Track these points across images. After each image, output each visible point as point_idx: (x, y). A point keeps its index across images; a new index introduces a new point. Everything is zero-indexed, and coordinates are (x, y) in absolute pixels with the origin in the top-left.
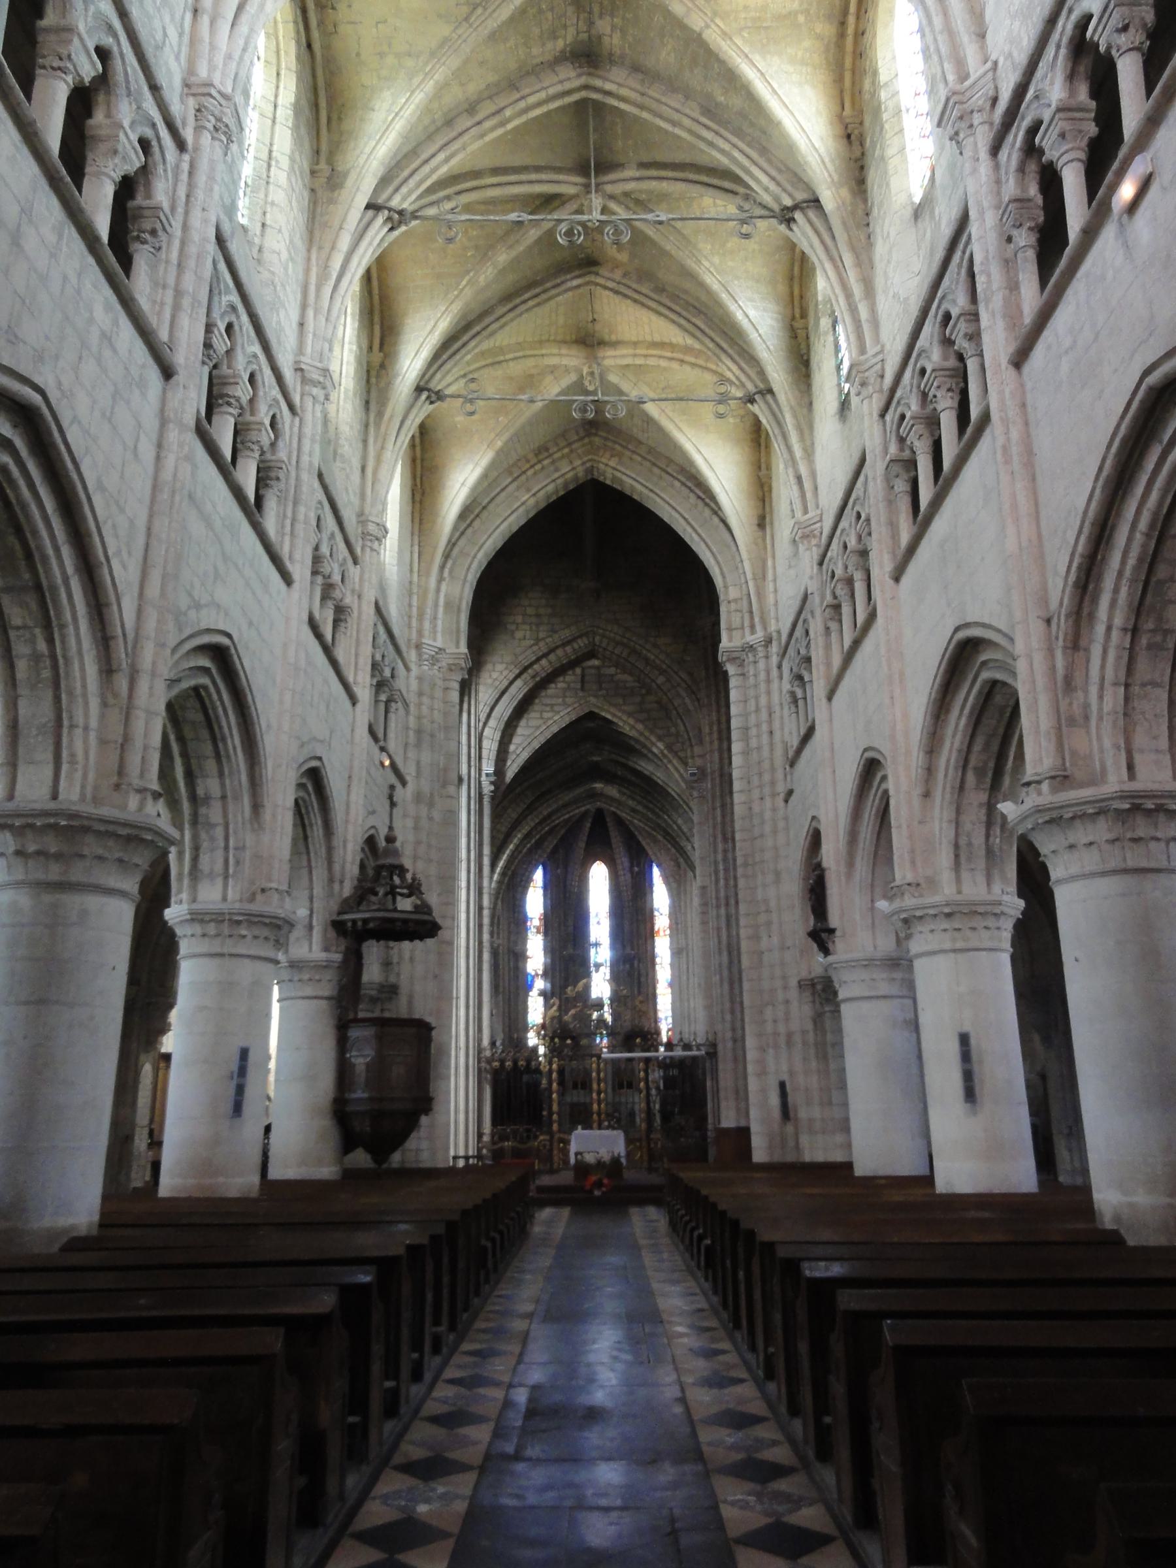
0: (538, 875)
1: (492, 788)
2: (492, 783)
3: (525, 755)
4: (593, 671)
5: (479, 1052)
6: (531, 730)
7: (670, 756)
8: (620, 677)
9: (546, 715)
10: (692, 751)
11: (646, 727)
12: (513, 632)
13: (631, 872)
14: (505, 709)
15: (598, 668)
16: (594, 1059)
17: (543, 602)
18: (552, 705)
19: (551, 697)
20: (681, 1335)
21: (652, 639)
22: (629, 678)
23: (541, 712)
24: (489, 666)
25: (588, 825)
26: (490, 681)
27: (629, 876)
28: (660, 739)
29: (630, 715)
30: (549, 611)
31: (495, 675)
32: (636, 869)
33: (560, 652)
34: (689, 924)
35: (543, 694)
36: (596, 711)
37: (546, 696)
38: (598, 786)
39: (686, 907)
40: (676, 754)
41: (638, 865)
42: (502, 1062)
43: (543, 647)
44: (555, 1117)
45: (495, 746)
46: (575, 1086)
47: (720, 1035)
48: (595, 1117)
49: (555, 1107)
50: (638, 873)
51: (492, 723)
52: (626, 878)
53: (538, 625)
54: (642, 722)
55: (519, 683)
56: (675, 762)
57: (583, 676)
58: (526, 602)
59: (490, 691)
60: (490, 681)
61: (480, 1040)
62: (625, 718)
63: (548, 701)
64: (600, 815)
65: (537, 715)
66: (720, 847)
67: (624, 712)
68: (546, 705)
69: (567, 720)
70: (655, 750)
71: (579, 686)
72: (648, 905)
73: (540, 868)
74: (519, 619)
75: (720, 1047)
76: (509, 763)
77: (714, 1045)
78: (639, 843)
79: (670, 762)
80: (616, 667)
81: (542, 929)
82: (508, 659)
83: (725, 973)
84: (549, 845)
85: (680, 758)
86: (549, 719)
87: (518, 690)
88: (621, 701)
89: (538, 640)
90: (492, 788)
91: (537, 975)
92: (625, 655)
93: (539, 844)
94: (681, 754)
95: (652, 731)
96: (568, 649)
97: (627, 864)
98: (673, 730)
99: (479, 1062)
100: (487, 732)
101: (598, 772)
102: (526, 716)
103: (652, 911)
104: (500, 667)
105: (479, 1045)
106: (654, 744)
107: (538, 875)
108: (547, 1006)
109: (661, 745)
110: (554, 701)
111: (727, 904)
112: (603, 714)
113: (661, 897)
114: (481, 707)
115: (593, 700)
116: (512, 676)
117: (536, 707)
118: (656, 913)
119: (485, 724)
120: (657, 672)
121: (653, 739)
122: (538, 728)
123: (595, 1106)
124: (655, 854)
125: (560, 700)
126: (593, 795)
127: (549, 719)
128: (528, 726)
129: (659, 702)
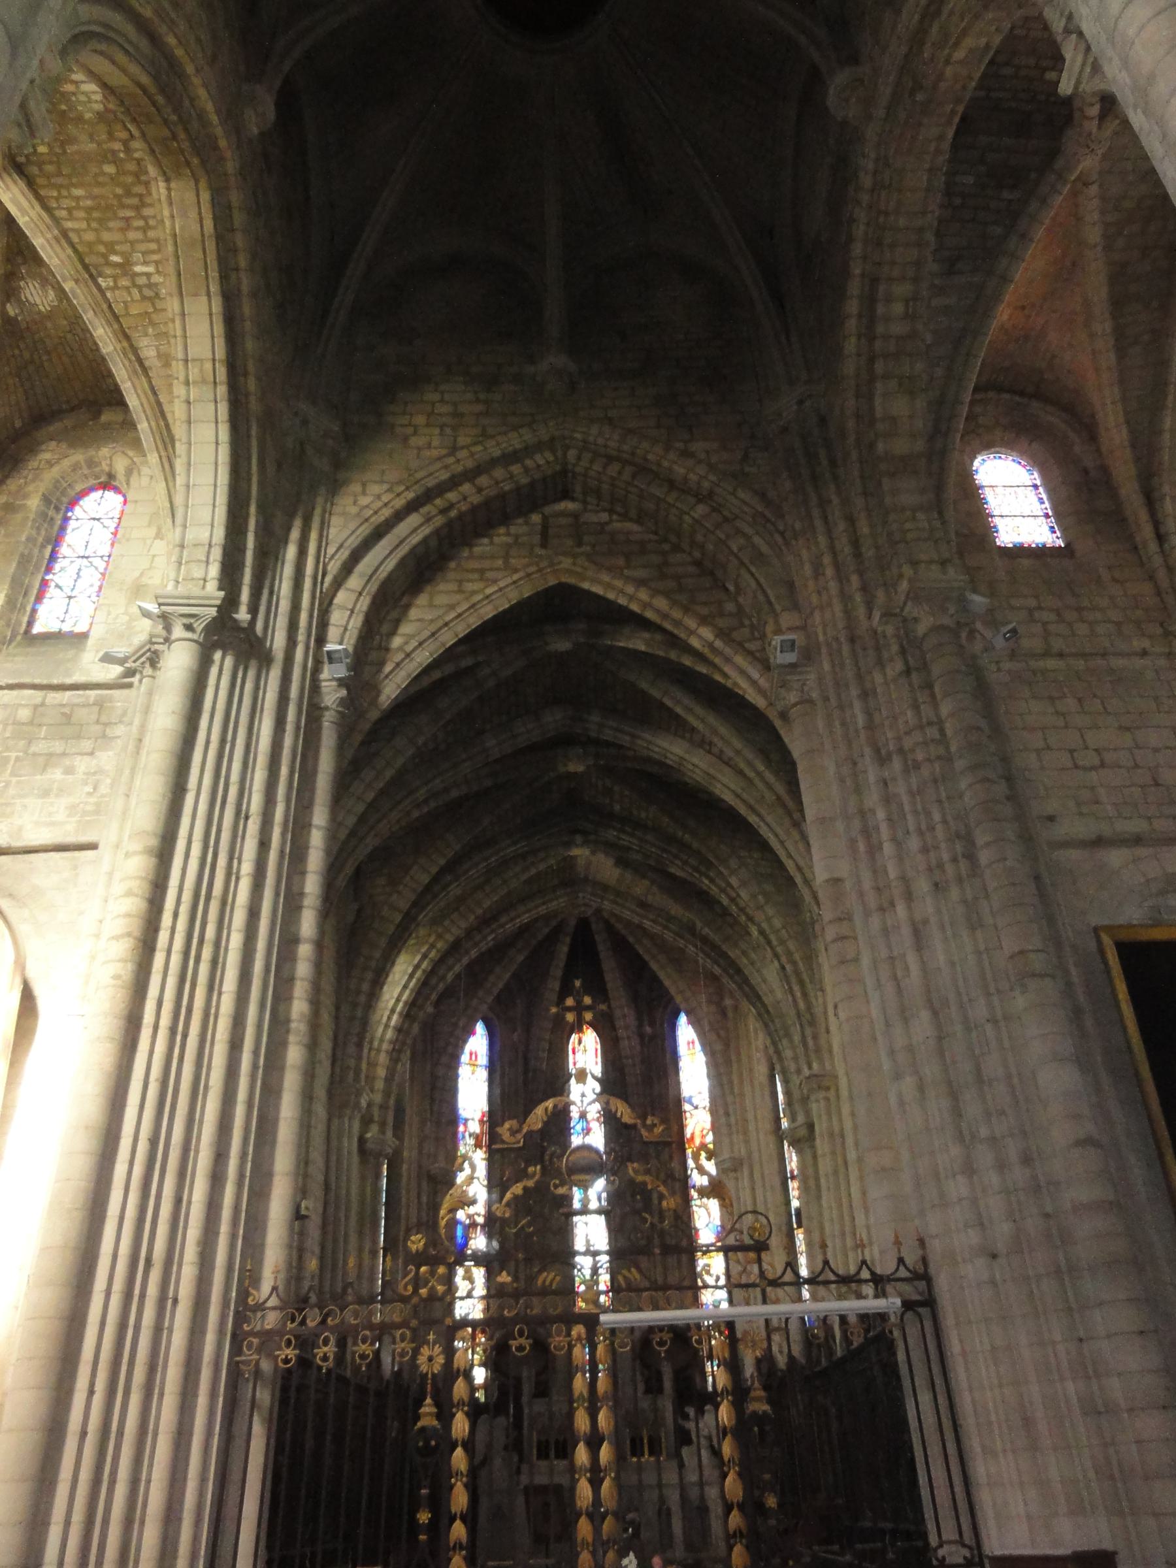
0: (478, 1043)
1: (344, 692)
2: (342, 682)
3: (423, 657)
4: (563, 521)
5: (241, 1318)
6: (440, 612)
7: (728, 651)
8: (617, 525)
9: (469, 586)
10: (777, 622)
11: (674, 603)
12: (406, 439)
13: (641, 1036)
14: (382, 559)
15: (575, 516)
16: (578, 1330)
17: (469, 396)
18: (482, 572)
19: (482, 557)
20: (137, 150)
21: (680, 445)
22: (635, 527)
23: (460, 582)
24: (356, 488)
25: (565, 949)
26: (354, 510)
27: (635, 1042)
28: (704, 620)
29: (641, 583)
30: (479, 408)
31: (364, 501)
32: (648, 1030)
33: (499, 473)
34: (750, 1116)
35: (466, 553)
36: (572, 580)
37: (471, 557)
38: (580, 852)
39: (741, 1082)
40: (740, 646)
41: (652, 1024)
42: (305, 1343)
43: (464, 461)
44: (459, 1531)
45: (357, 622)
46: (543, 1454)
47: (936, 1247)
48: (584, 1528)
49: (460, 1499)
50: (653, 1038)
51: (354, 582)
52: (630, 1045)
53: (454, 428)
54: (667, 594)
55: (414, 519)
56: (739, 659)
57: (545, 527)
58: (436, 397)
59: (352, 526)
60: (354, 510)
61: (250, 1277)
62: (630, 589)
63: (475, 565)
64: (584, 925)
65: (453, 586)
66: (872, 774)
67: (628, 579)
68: (473, 571)
69: (514, 596)
70: (695, 642)
71: (537, 539)
72: (671, 1092)
73: (480, 1028)
74: (420, 420)
75: (943, 1284)
76: (388, 668)
77: (922, 1276)
78: (655, 979)
79: (728, 660)
80: (611, 511)
81: (485, 1140)
82: (392, 476)
83: (931, 1071)
84: (500, 979)
85: (750, 653)
86: (474, 593)
87: (412, 531)
88: (621, 562)
89: (454, 450)
90: (344, 692)
91: (474, 1225)
92: (626, 476)
93: (476, 974)
94: (752, 646)
95: (686, 610)
96: (516, 469)
97: (632, 1020)
98: (730, 607)
99: (236, 1349)
100: (341, 597)
101: (575, 813)
102: (428, 588)
103: (678, 1101)
104: (375, 489)
105: (243, 1294)
106: (692, 633)
107: (478, 1043)
108: (302, 887)
109: (707, 633)
110: (487, 564)
111: (909, 897)
112: (586, 585)
113: (694, 1074)
114: (331, 550)
115: (566, 562)
116: (399, 503)
117: (451, 575)
118: (687, 1107)
119: (338, 583)
120: (692, 500)
121: (691, 623)
122: (452, 607)
123: (584, 1490)
124: (686, 1000)
125: (500, 562)
126: (568, 878)
127: (474, 593)
128: (431, 605)
129: (698, 564)
